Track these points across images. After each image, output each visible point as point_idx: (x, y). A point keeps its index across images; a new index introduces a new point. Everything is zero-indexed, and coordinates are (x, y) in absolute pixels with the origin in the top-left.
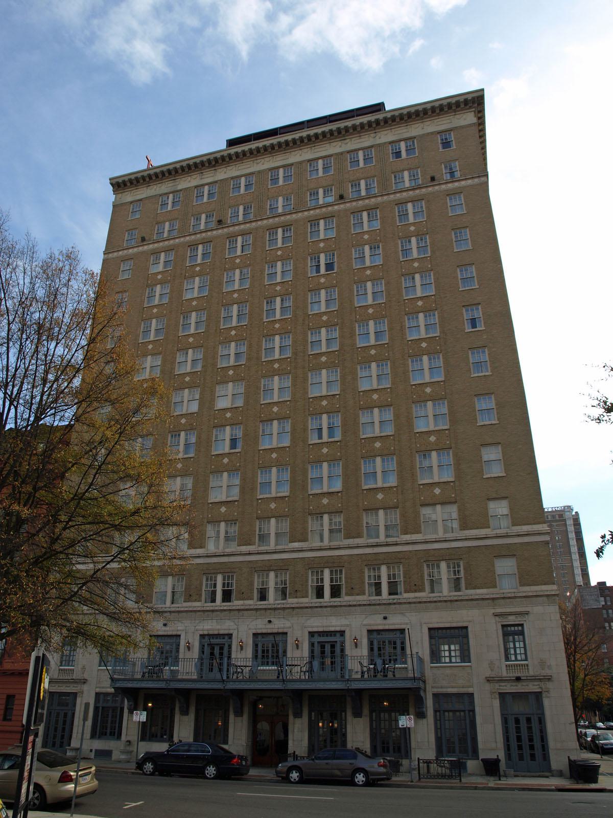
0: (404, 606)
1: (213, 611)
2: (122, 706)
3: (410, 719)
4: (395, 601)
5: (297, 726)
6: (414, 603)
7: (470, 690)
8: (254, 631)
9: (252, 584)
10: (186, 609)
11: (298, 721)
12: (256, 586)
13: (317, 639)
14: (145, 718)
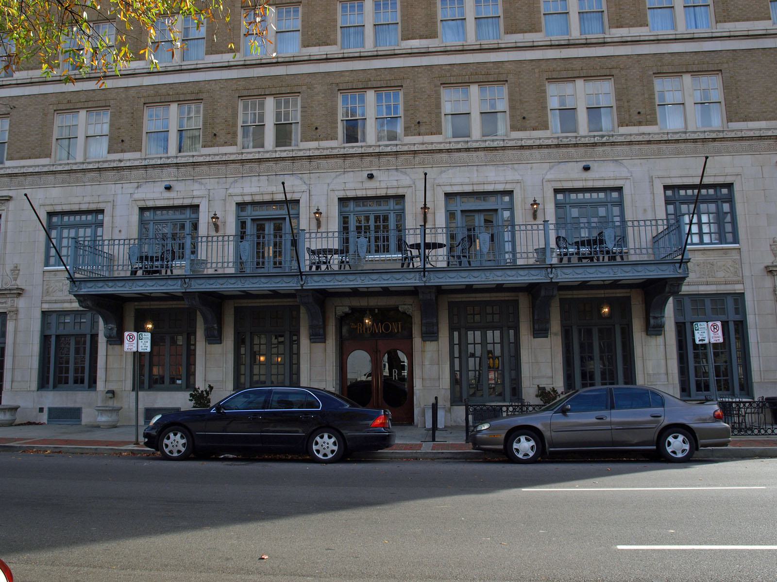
0: (619, 148)
1: (260, 161)
2: (94, 332)
3: (715, 327)
4: (604, 140)
5: (428, 355)
6: (639, 143)
7: (738, 288)
8: (342, 194)
9: (333, 112)
10: (208, 159)
11: (431, 346)
12: (340, 117)
13: (459, 205)
14: (149, 344)
